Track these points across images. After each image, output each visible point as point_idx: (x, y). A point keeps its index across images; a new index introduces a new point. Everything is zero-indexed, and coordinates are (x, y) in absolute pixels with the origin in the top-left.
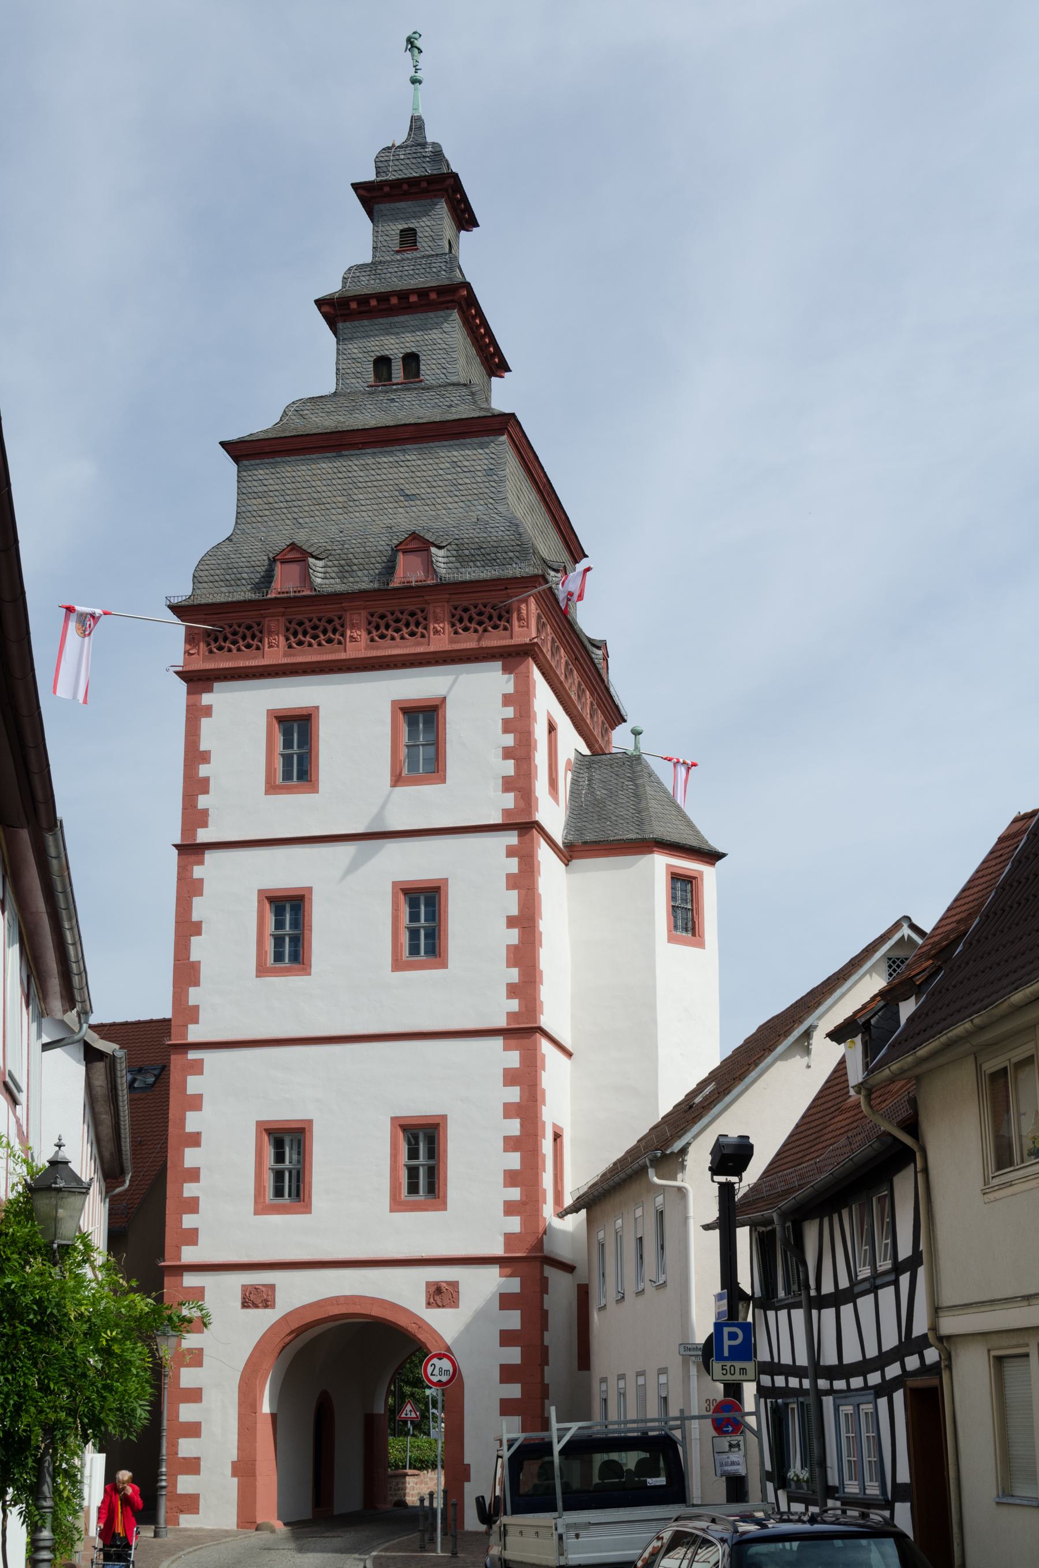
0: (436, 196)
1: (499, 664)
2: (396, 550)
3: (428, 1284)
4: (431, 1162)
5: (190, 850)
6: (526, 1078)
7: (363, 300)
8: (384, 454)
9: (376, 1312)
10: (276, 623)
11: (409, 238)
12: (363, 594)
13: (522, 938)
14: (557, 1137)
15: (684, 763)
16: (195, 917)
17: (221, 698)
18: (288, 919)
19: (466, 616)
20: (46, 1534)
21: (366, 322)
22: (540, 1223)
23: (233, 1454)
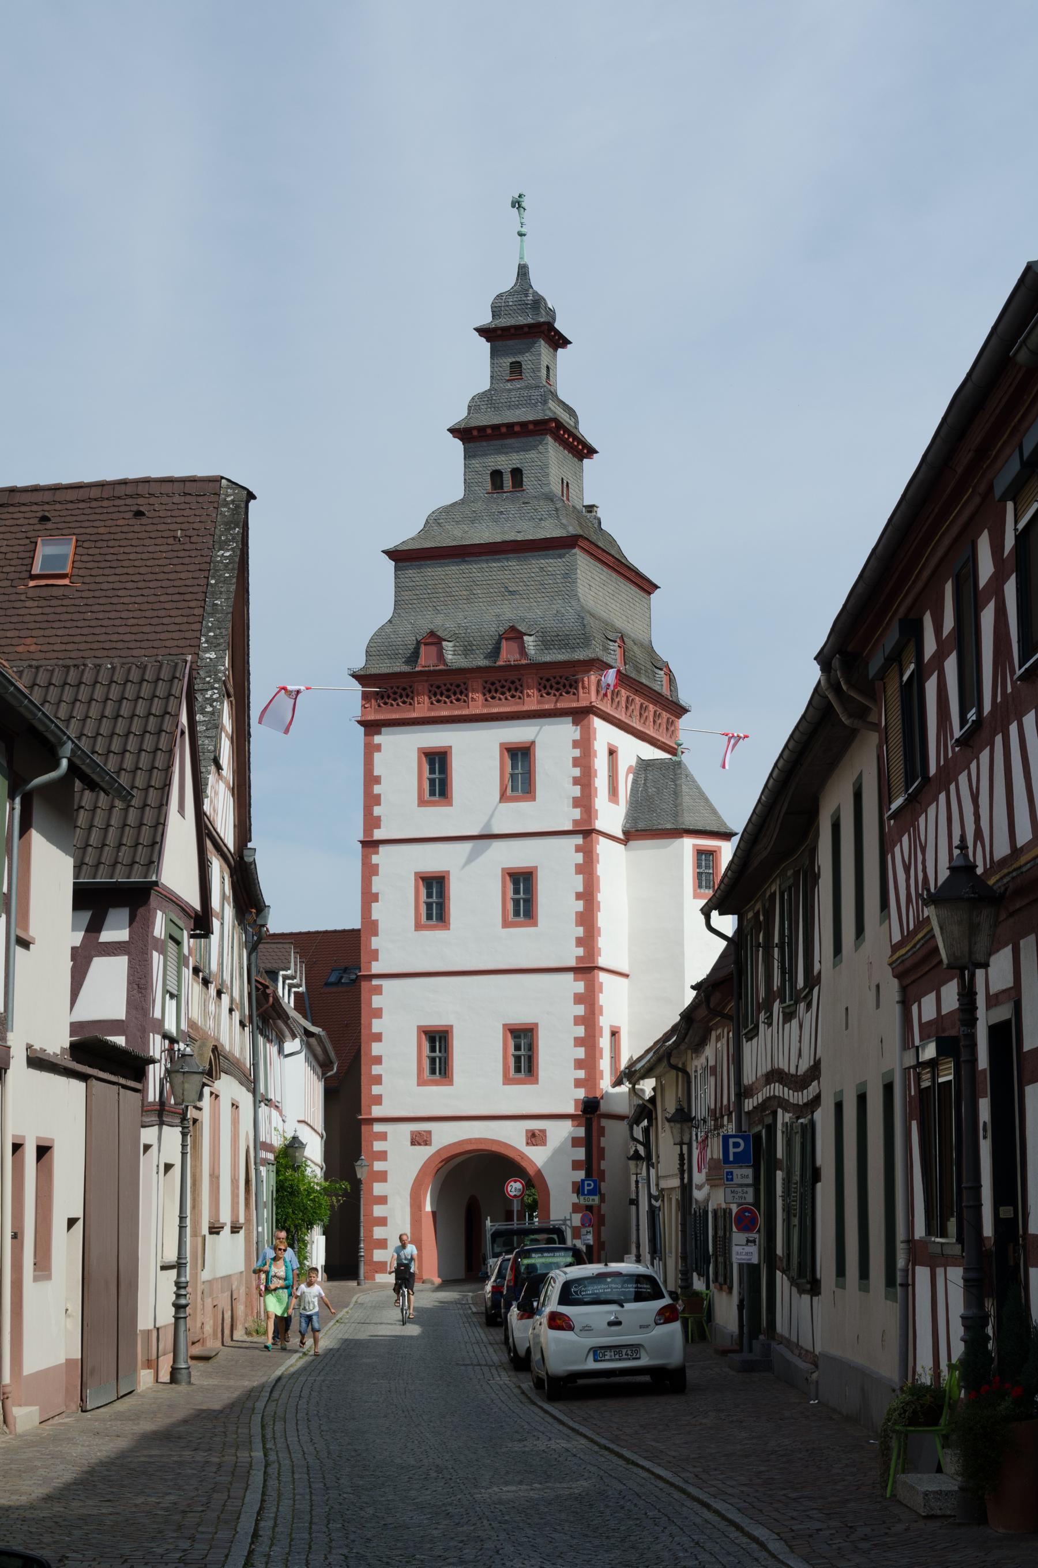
1: (570, 719)
2: (501, 637)
5: (370, 845)
6: (589, 1000)
9: (494, 1148)
11: (516, 368)
12: (479, 669)
13: (586, 906)
14: (614, 1034)
16: (374, 890)
17: (385, 739)
18: (434, 888)
21: (484, 444)
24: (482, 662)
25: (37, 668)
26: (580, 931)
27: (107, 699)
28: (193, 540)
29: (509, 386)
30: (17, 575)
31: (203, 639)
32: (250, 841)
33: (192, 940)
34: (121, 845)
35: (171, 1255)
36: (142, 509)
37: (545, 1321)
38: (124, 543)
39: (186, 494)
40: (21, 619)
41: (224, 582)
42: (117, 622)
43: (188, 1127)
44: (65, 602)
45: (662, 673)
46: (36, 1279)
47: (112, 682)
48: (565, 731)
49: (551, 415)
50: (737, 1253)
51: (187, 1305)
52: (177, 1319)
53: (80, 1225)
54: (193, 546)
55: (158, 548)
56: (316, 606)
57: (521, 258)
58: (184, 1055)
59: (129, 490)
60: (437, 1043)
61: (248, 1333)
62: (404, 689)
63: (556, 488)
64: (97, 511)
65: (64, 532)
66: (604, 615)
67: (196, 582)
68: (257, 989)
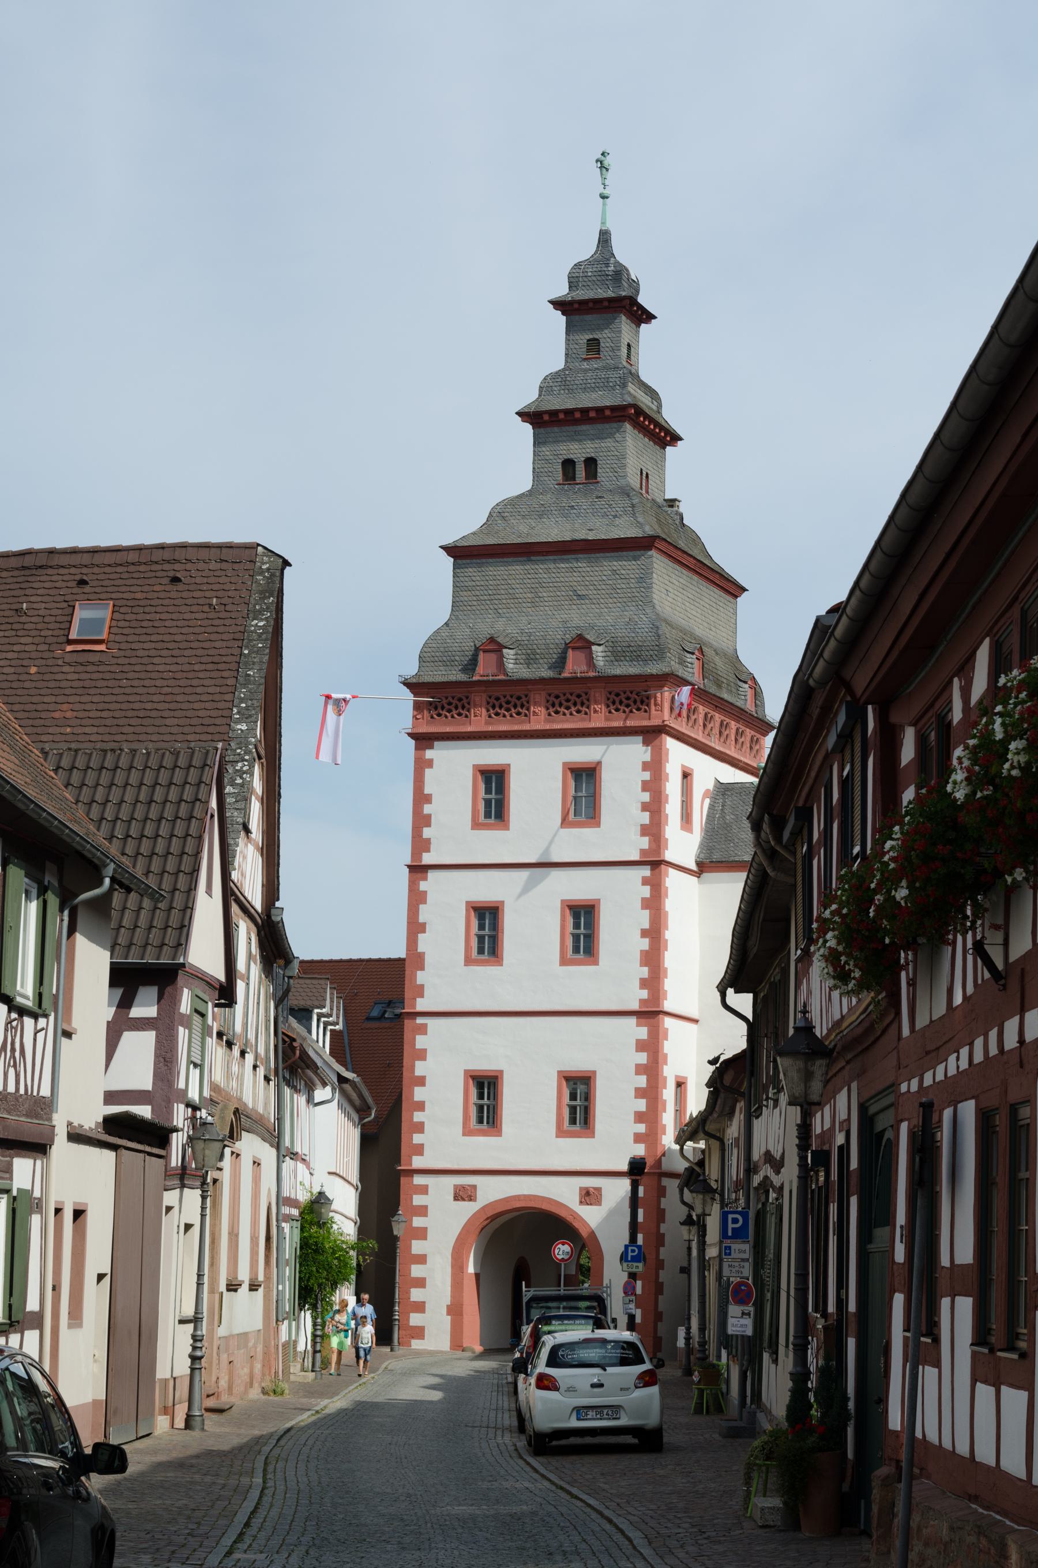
0: (615, 311)
1: (640, 738)
3: (581, 1189)
4: (586, 1104)
5: (418, 870)
6: (652, 1048)
8: (563, 561)
9: (545, 1206)
10: (479, 698)
11: (594, 346)
12: (542, 681)
14: (680, 1084)
16: (421, 920)
17: (437, 753)
18: (487, 919)
19: (617, 700)
20: (319, 1320)
21: (556, 429)
22: (659, 1147)
23: (448, 1300)
24: (546, 673)
25: (76, 751)
26: (645, 972)
27: (142, 784)
28: (228, 608)
29: (585, 365)
30: (55, 640)
31: (235, 710)
32: (278, 899)
33: (216, 1009)
34: (151, 927)
35: (189, 1311)
36: (178, 575)
37: (533, 1381)
38: (159, 609)
39: (222, 561)
40: (57, 684)
41: (257, 653)
42: (152, 690)
43: (208, 1188)
44: (101, 668)
45: (746, 686)
46: (70, 1326)
47: (146, 767)
49: (629, 400)
50: (733, 1325)
51: (202, 1357)
52: (193, 1369)
53: (108, 1279)
54: (228, 615)
55: (193, 616)
56: (363, 618)
57: (603, 223)
58: (205, 1124)
59: (167, 555)
60: (486, 1087)
61: (264, 1392)
62: (460, 700)
63: (634, 481)
64: (134, 575)
65: (102, 596)
66: (683, 623)
67: (229, 651)
68: (284, 1042)
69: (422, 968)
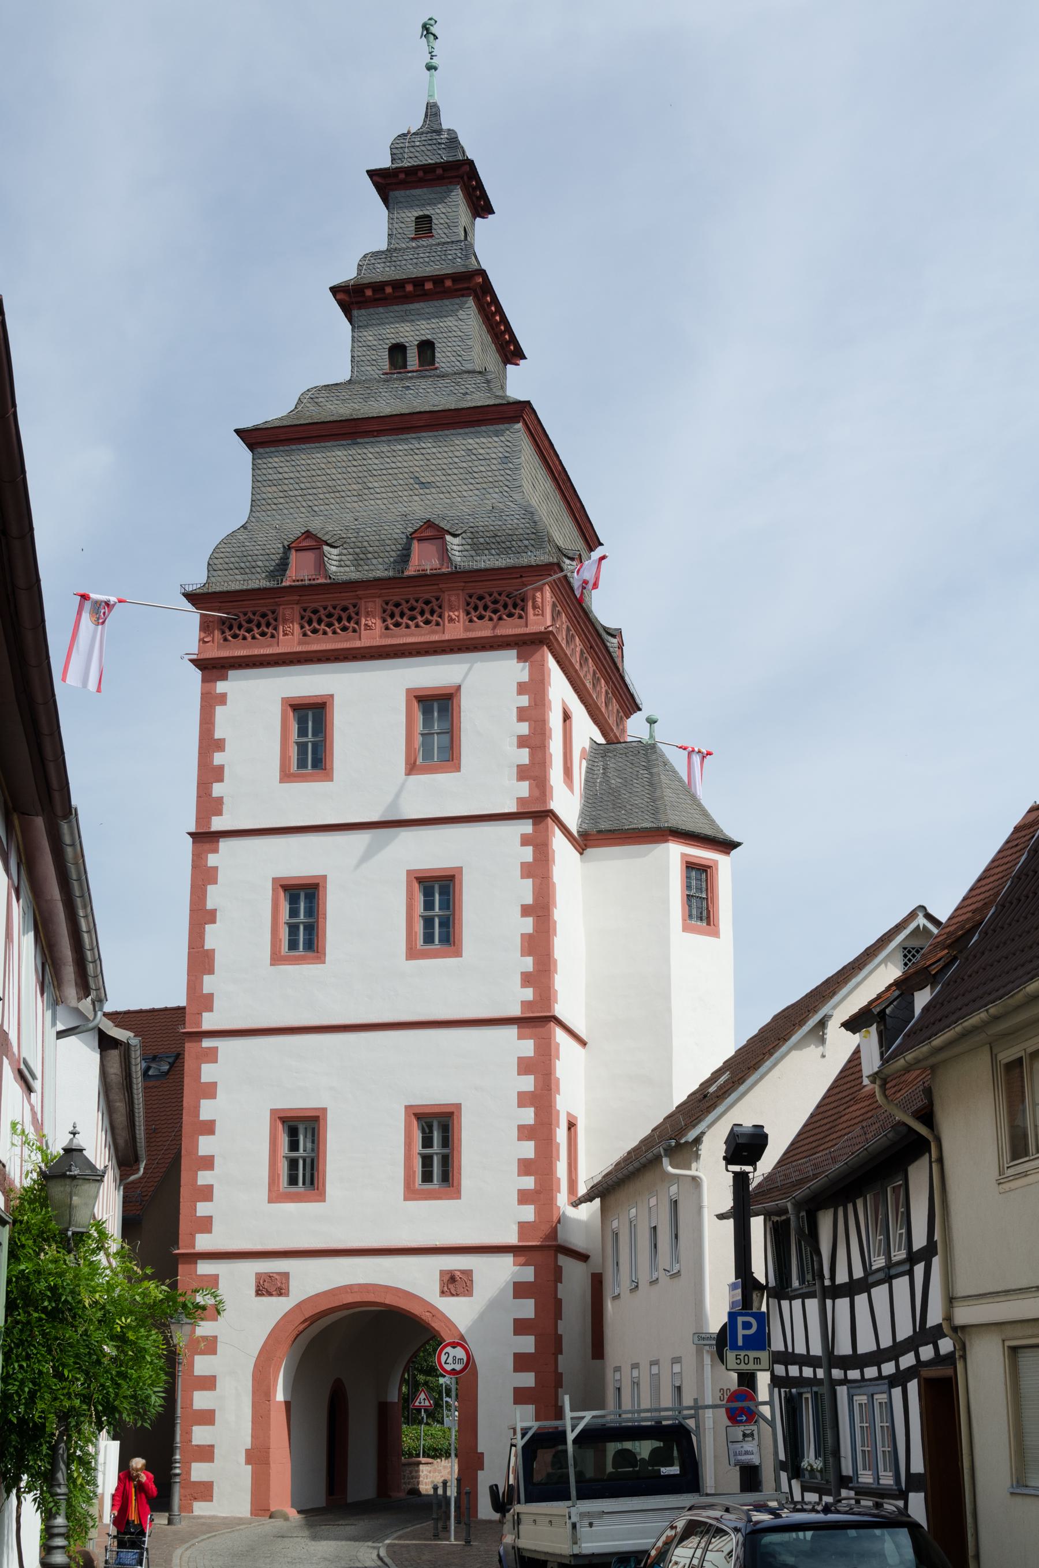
0: (451, 183)
1: (514, 653)
2: (411, 538)
3: (442, 1273)
4: (445, 1151)
5: (205, 838)
6: (541, 1067)
7: (378, 287)
11: (424, 225)
14: (571, 1126)
15: (699, 752)
16: (210, 906)
21: (381, 309)
23: (247, 1442)
48: (505, 670)
69: (211, 971)
